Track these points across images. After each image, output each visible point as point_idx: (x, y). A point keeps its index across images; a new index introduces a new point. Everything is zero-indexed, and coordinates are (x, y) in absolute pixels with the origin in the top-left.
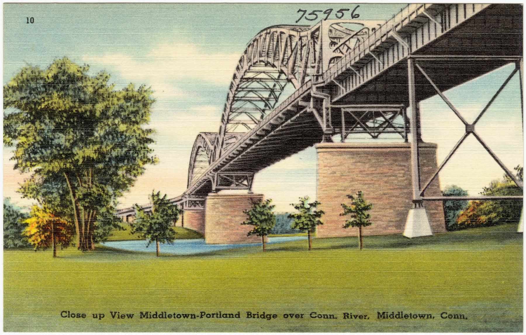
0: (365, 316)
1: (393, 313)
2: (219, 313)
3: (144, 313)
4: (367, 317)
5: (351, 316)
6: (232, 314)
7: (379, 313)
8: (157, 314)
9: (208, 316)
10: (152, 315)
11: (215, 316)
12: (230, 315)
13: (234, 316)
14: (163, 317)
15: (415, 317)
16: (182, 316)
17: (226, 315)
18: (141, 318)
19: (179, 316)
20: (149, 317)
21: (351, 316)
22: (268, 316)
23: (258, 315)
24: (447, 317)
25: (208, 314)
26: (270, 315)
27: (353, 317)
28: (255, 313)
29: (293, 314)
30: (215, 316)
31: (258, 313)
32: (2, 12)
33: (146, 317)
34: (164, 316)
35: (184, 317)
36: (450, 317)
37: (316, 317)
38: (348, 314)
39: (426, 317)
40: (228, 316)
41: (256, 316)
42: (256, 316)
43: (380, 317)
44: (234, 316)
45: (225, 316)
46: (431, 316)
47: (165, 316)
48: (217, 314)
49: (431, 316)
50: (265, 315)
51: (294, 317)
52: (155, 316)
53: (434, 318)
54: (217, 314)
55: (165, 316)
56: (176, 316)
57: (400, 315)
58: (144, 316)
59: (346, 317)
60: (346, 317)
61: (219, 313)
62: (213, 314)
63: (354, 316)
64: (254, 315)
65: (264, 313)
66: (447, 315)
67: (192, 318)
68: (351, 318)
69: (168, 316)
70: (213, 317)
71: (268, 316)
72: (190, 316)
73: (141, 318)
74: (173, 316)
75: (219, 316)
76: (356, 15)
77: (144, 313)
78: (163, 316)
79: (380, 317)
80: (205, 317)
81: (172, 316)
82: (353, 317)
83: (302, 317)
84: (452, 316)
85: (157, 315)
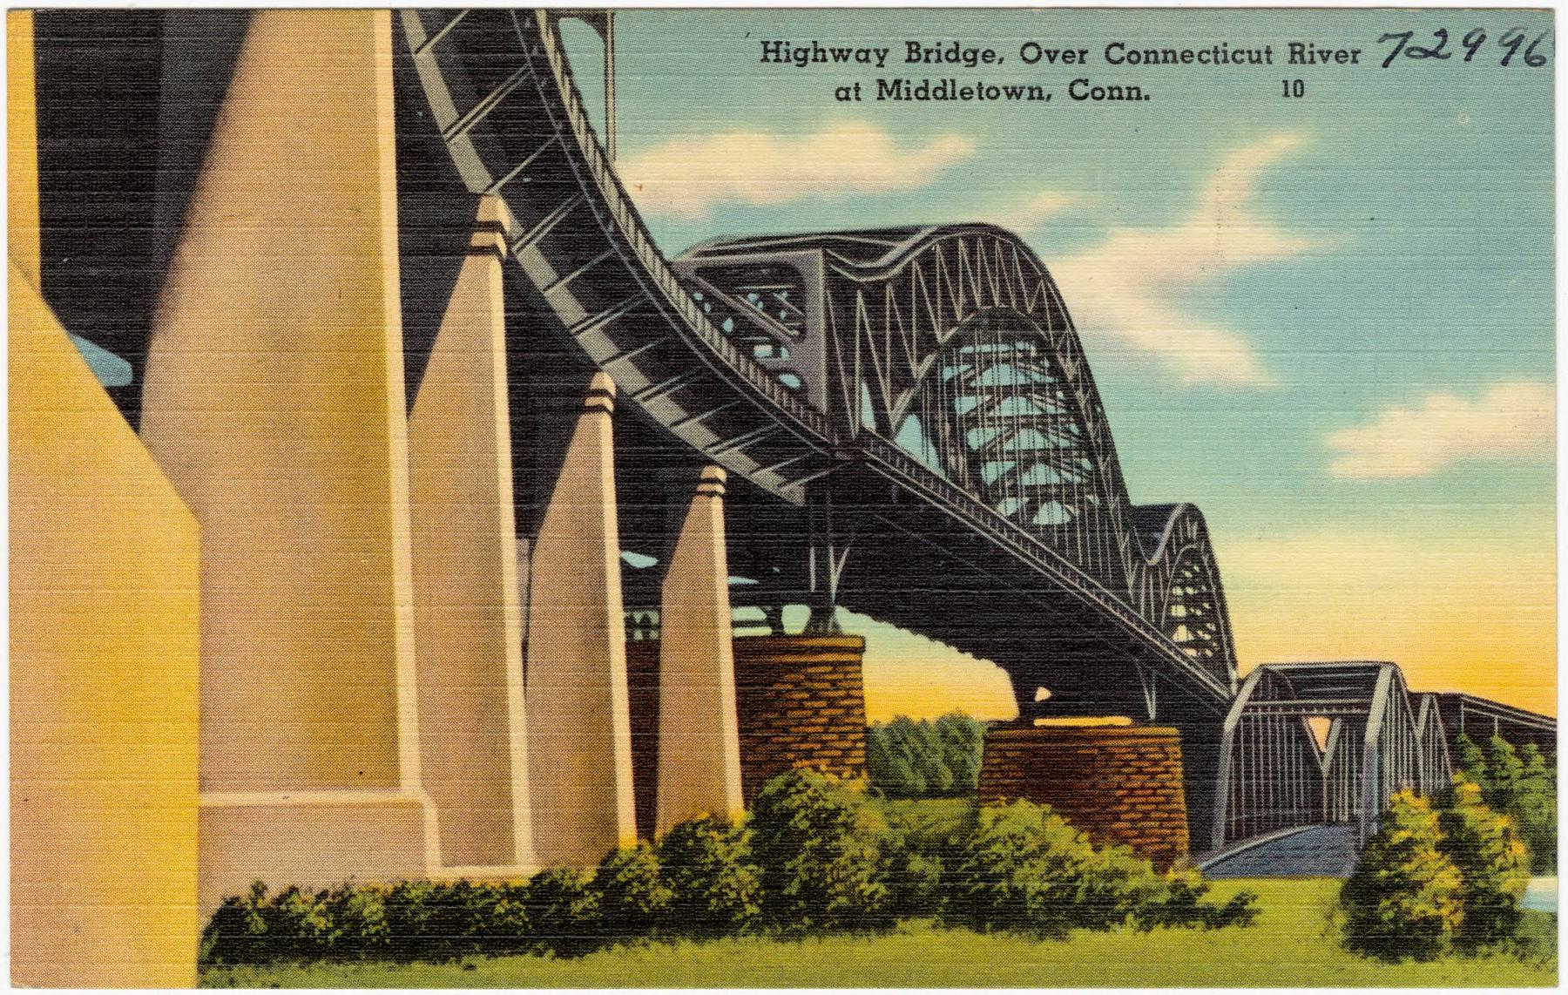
2: (1221, 48)
5: (1312, 53)
6: (1173, 52)
8: (957, 48)
10: (792, 51)
14: (944, 97)
15: (993, 93)
16: (1002, 92)
18: (881, 98)
19: (1187, 56)
22: (970, 56)
23: (939, 52)
26: (975, 52)
27: (1317, 57)
28: (929, 48)
29: (1329, 52)
31: (939, 44)
33: (894, 94)
34: (949, 94)
35: (1009, 96)
37: (1085, 97)
38: (1302, 46)
39: (1026, 93)
41: (933, 56)
42: (933, 56)
43: (885, 94)
44: (1107, 94)
46: (1139, 94)
47: (953, 95)
49: (1139, 94)
55: (953, 95)
57: (949, 88)
58: (890, 94)
59: (1297, 57)
63: (1321, 52)
64: (928, 52)
65: (957, 44)
67: (1031, 98)
68: (1312, 61)
71: (970, 56)
73: (881, 98)
75: (1221, 57)
76: (1537, 57)
78: (945, 95)
79: (885, 94)
81: (972, 92)
82: (1317, 57)
84: (1139, 57)
85: (957, 54)
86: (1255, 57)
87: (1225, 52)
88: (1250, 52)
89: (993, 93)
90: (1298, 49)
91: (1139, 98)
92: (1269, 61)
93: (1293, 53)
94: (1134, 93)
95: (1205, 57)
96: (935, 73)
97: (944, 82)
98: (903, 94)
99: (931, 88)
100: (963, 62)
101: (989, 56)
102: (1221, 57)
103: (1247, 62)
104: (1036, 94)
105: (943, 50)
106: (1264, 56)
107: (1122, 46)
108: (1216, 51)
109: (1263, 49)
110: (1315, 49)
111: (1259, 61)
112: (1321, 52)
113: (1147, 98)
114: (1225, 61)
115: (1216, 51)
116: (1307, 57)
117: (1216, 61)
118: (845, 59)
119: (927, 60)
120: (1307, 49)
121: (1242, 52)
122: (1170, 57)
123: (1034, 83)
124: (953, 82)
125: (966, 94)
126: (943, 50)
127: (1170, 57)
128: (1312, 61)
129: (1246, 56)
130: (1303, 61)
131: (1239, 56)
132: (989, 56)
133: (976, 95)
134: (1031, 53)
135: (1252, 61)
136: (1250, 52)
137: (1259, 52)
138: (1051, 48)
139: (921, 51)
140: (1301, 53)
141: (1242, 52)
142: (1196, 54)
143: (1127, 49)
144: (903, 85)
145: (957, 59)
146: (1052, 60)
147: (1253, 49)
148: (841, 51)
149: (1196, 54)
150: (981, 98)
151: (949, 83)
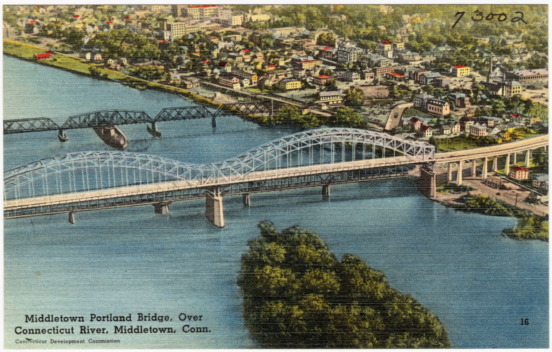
0: (104, 329)
1: (156, 314)
2: (56, 328)
3: (30, 317)
4: (105, 331)
5: (88, 330)
6: (123, 317)
7: (27, 316)
9: (99, 319)
11: (106, 319)
12: (121, 317)
13: (125, 319)
16: (69, 319)
17: (117, 317)
20: (124, 331)
21: (88, 330)
22: (160, 318)
24: (21, 332)
25: (65, 318)
26: (162, 317)
27: (90, 331)
30: (106, 319)
31: (149, 314)
32: (3, 317)
34: (140, 331)
36: (25, 332)
40: (119, 319)
43: (117, 331)
45: (115, 319)
48: (108, 317)
50: (157, 316)
51: (95, 331)
52: (130, 331)
53: (107, 332)
54: (108, 317)
56: (63, 319)
58: (30, 320)
59: (83, 331)
60: (83, 331)
61: (109, 316)
62: (104, 317)
63: (91, 329)
64: (145, 317)
65: (42, 315)
66: (21, 330)
69: (144, 330)
70: (104, 320)
72: (167, 331)
74: (60, 319)
75: (56, 331)
77: (30, 317)
80: (95, 320)
82: (90, 331)
83: (200, 320)
86: (68, 331)
87: (57, 330)
88: (66, 329)
89: (155, 330)
90: (83, 328)
91: (207, 331)
92: (73, 333)
93: (82, 330)
94: (205, 330)
95: (50, 331)
96: (146, 324)
97: (138, 327)
98: (124, 331)
99: (133, 329)
100: (158, 321)
101: (167, 318)
102: (56, 331)
103: (65, 333)
104: (170, 330)
105: (151, 316)
106: (71, 331)
107: (21, 328)
108: (54, 329)
109: (70, 328)
110: (89, 328)
111: (69, 332)
112: (91, 329)
113: (210, 331)
114: (57, 333)
115: (54, 329)
116: (87, 331)
117: (54, 333)
118: (75, 320)
119: (145, 320)
120: (87, 328)
121: (63, 330)
122: (38, 331)
123: (170, 327)
124: (141, 327)
125: (146, 330)
126: (151, 316)
127: (38, 331)
128: (88, 333)
129: (64, 331)
130: (85, 333)
131: (62, 331)
132: (167, 318)
133: (149, 331)
134: (183, 317)
135: (66, 333)
136: (66, 329)
137: (69, 329)
138: (190, 315)
139: (143, 317)
140: (84, 330)
141: (63, 330)
142: (47, 330)
143: (23, 329)
144: (123, 328)
145: (156, 320)
146: (190, 319)
147: (67, 328)
148: (73, 318)
149: (47, 330)
150: (151, 332)
151: (140, 328)
